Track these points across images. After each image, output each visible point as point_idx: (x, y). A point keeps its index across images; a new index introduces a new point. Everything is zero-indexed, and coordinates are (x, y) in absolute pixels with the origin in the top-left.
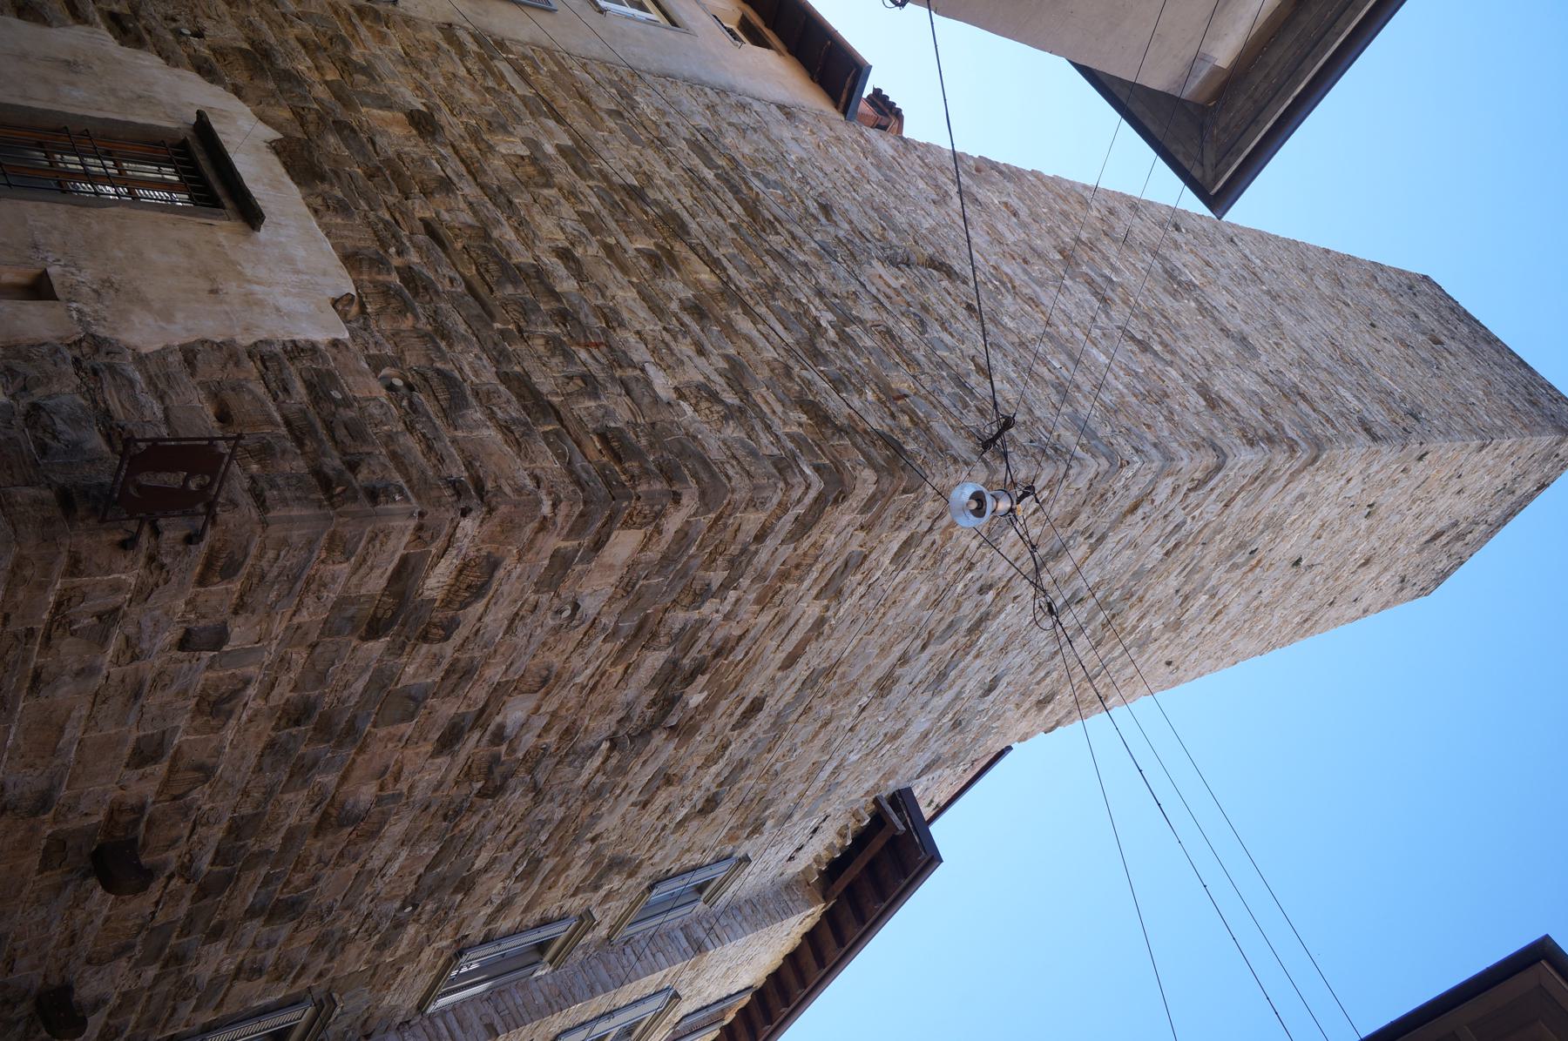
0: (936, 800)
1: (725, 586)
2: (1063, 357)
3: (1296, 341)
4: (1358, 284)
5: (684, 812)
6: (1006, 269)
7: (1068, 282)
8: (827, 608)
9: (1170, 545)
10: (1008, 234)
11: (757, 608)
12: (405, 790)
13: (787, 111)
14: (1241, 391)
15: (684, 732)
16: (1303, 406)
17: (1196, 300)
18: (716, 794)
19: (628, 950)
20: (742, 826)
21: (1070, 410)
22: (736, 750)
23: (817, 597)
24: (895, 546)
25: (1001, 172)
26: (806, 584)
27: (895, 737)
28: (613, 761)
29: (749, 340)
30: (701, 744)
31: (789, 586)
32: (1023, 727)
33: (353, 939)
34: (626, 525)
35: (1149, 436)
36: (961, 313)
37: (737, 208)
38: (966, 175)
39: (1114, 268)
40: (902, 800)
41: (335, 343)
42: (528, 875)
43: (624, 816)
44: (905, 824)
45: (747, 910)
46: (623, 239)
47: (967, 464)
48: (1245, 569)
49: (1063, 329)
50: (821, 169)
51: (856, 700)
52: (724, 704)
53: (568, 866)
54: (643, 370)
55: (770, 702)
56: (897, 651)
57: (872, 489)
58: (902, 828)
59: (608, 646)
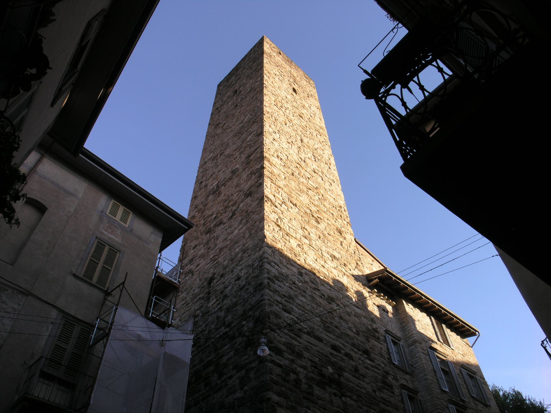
0: (371, 262)
1: (295, 373)
2: (236, 246)
3: (234, 151)
4: (219, 116)
7: (215, 235)
8: (304, 332)
14: (246, 181)
15: (340, 370)
16: (252, 158)
17: (222, 186)
19: (415, 366)
20: (374, 336)
22: (348, 349)
23: (300, 337)
24: (287, 314)
25: (184, 246)
26: (296, 343)
28: (349, 394)
29: (228, 360)
31: (296, 349)
35: (257, 223)
36: (223, 280)
43: (367, 384)
44: (376, 278)
45: (403, 324)
47: (262, 296)
49: (228, 243)
52: (333, 359)
53: (384, 399)
54: (235, 399)
56: (319, 300)
58: (377, 280)
59: (312, 408)
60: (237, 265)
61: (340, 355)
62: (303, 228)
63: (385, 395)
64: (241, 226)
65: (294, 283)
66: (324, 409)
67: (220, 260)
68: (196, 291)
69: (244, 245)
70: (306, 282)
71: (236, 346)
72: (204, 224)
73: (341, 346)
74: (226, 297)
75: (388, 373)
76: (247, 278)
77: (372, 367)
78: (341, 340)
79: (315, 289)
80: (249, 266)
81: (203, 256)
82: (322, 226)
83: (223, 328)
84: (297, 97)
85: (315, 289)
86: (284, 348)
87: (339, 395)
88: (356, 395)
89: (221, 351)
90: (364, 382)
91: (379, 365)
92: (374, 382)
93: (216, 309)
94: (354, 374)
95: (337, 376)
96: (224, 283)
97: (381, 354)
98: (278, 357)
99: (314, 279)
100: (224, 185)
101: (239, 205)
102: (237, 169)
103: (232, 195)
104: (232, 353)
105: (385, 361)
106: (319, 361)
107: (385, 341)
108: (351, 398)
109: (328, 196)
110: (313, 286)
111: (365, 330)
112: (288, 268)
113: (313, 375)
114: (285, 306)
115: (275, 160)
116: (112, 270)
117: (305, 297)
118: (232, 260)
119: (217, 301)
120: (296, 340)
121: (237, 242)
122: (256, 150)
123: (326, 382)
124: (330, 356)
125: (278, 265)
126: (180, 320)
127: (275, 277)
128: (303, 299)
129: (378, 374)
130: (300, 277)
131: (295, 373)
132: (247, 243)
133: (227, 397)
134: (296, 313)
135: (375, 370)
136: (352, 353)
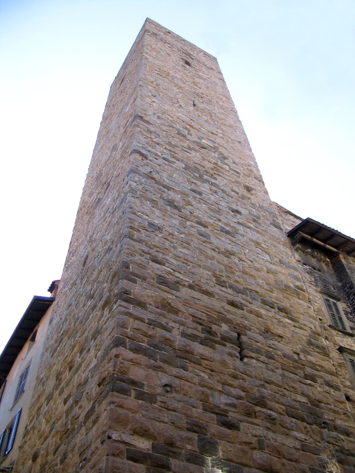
8: (184, 285)
9: (174, 160)
11: (180, 314)
12: (256, 439)
27: (257, 244)
28: (253, 355)
30: (251, 321)
32: (261, 194)
40: (291, 235)
42: (313, 378)
51: (235, 263)
55: (230, 298)
57: (125, 281)
63: (315, 358)
73: (243, 302)
87: (238, 355)
123: (209, 338)
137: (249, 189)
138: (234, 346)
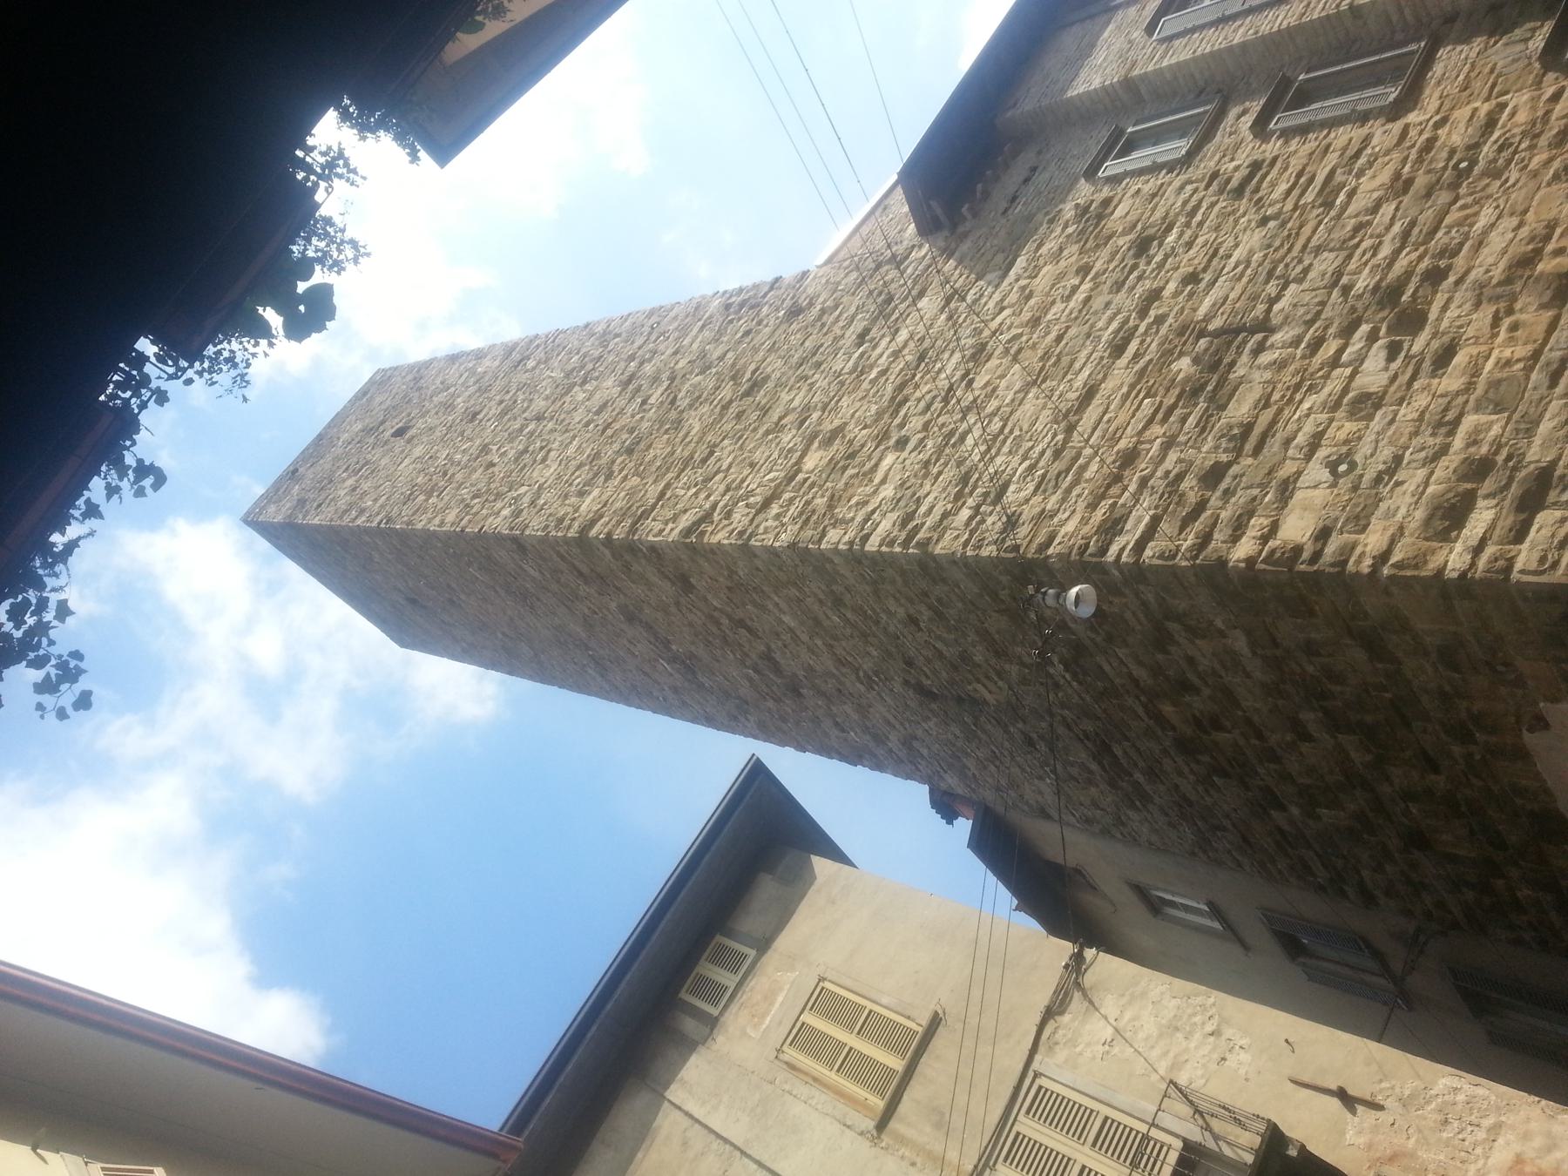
2: (826, 623)
5: (1170, 239)
6: (862, 688)
8: (1066, 441)
10: (849, 711)
13: (1044, 814)
16: (585, 569)
17: (670, 650)
18: (1138, 255)
21: (834, 588)
22: (1126, 301)
28: (1261, 308)
29: (1140, 663)
33: (1524, 134)
34: (1298, 550)
35: (758, 563)
37: (1118, 751)
38: (905, 762)
39: (750, 680)
41: (1555, 700)
43: (1237, 245)
46: (1242, 742)
48: (617, 426)
49: (819, 643)
50: (1023, 770)
52: (1153, 351)
54: (1254, 653)
60: (877, 623)
61: (1142, 329)
62: (778, 427)
64: (771, 607)
65: (926, 464)
66: (1298, 387)
67: (867, 665)
68: (958, 732)
69: (821, 601)
70: (926, 427)
71: (1099, 639)
72: (777, 700)
73: (1115, 325)
74: (965, 657)
75: (1215, 175)
76: (911, 602)
77: (1188, 225)
78: (1100, 324)
79: (946, 400)
80: (876, 592)
81: (863, 710)
82: (775, 366)
83: (1052, 671)
84: (420, 424)
85: (946, 400)
86: (1105, 504)
87: (1259, 337)
88: (1267, 282)
89: (1117, 681)
90: (1230, 256)
91: (1185, 203)
92: (1236, 222)
93: (1000, 683)
94: (1202, 285)
95: (1203, 343)
96: (929, 661)
97: (1154, 195)
98: (1128, 527)
99: (919, 400)
100: (667, 644)
101: (716, 609)
102: (623, 609)
103: (691, 625)
104: (1121, 652)
105: (1177, 183)
106: (1154, 396)
107: (1115, 180)
108: (1272, 301)
109: (695, 346)
110: (937, 405)
111: (1075, 248)
112: (883, 482)
113: (1192, 421)
114: (986, 495)
115: (588, 505)
116: (870, 1005)
117: (969, 431)
118: (864, 635)
119: (978, 681)
120: (1084, 468)
121: (817, 622)
122: (562, 558)
123: (1212, 384)
124: (1142, 363)
125: (873, 512)
126: (1040, 778)
127: (904, 523)
128: (970, 441)
129: (1213, 205)
130: (910, 446)
131: (1180, 477)
132: (815, 595)
133: (1248, 676)
134: (1007, 464)
135: (1199, 217)
136: (1139, 290)
137: (795, 312)
138: (1236, 343)
